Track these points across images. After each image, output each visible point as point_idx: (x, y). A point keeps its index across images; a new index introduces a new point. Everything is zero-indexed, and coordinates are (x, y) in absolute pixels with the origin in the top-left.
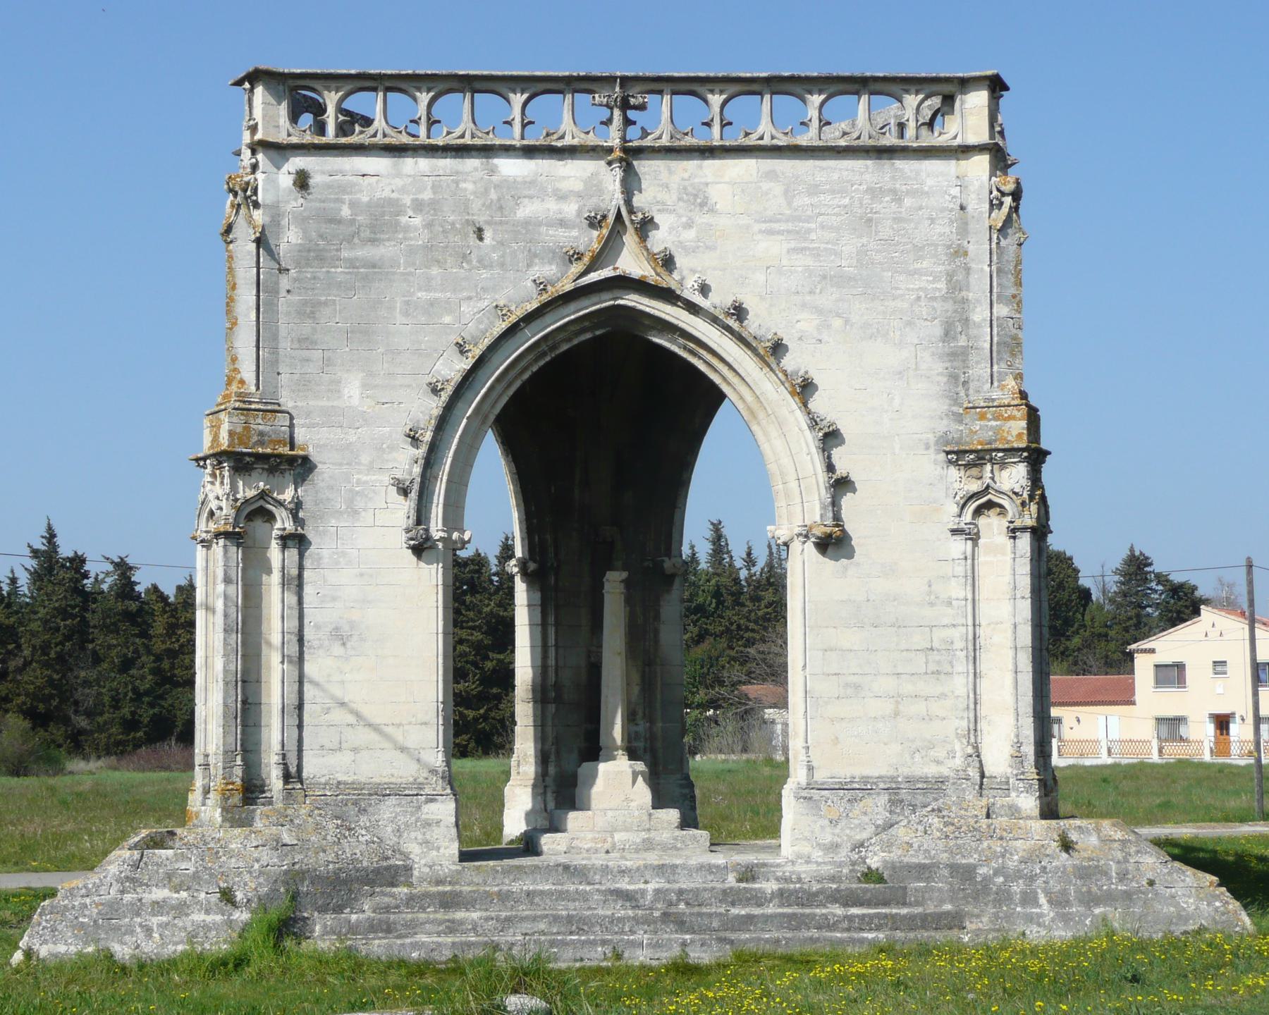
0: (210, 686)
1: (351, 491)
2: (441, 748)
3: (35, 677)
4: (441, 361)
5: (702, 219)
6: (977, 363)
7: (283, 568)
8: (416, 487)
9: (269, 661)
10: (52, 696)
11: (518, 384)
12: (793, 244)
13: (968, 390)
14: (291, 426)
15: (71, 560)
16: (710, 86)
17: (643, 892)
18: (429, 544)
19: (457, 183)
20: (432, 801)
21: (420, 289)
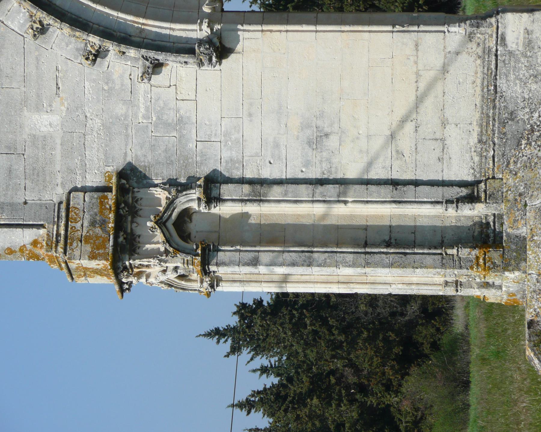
0: (370, 279)
1: (156, 126)
2: (444, 28)
3: (365, 356)
4: (9, 23)
7: (242, 201)
8: (152, 54)
9: (344, 217)
10: (386, 340)
14: (84, 190)
15: (242, 318)
18: (216, 40)
20: (503, 39)
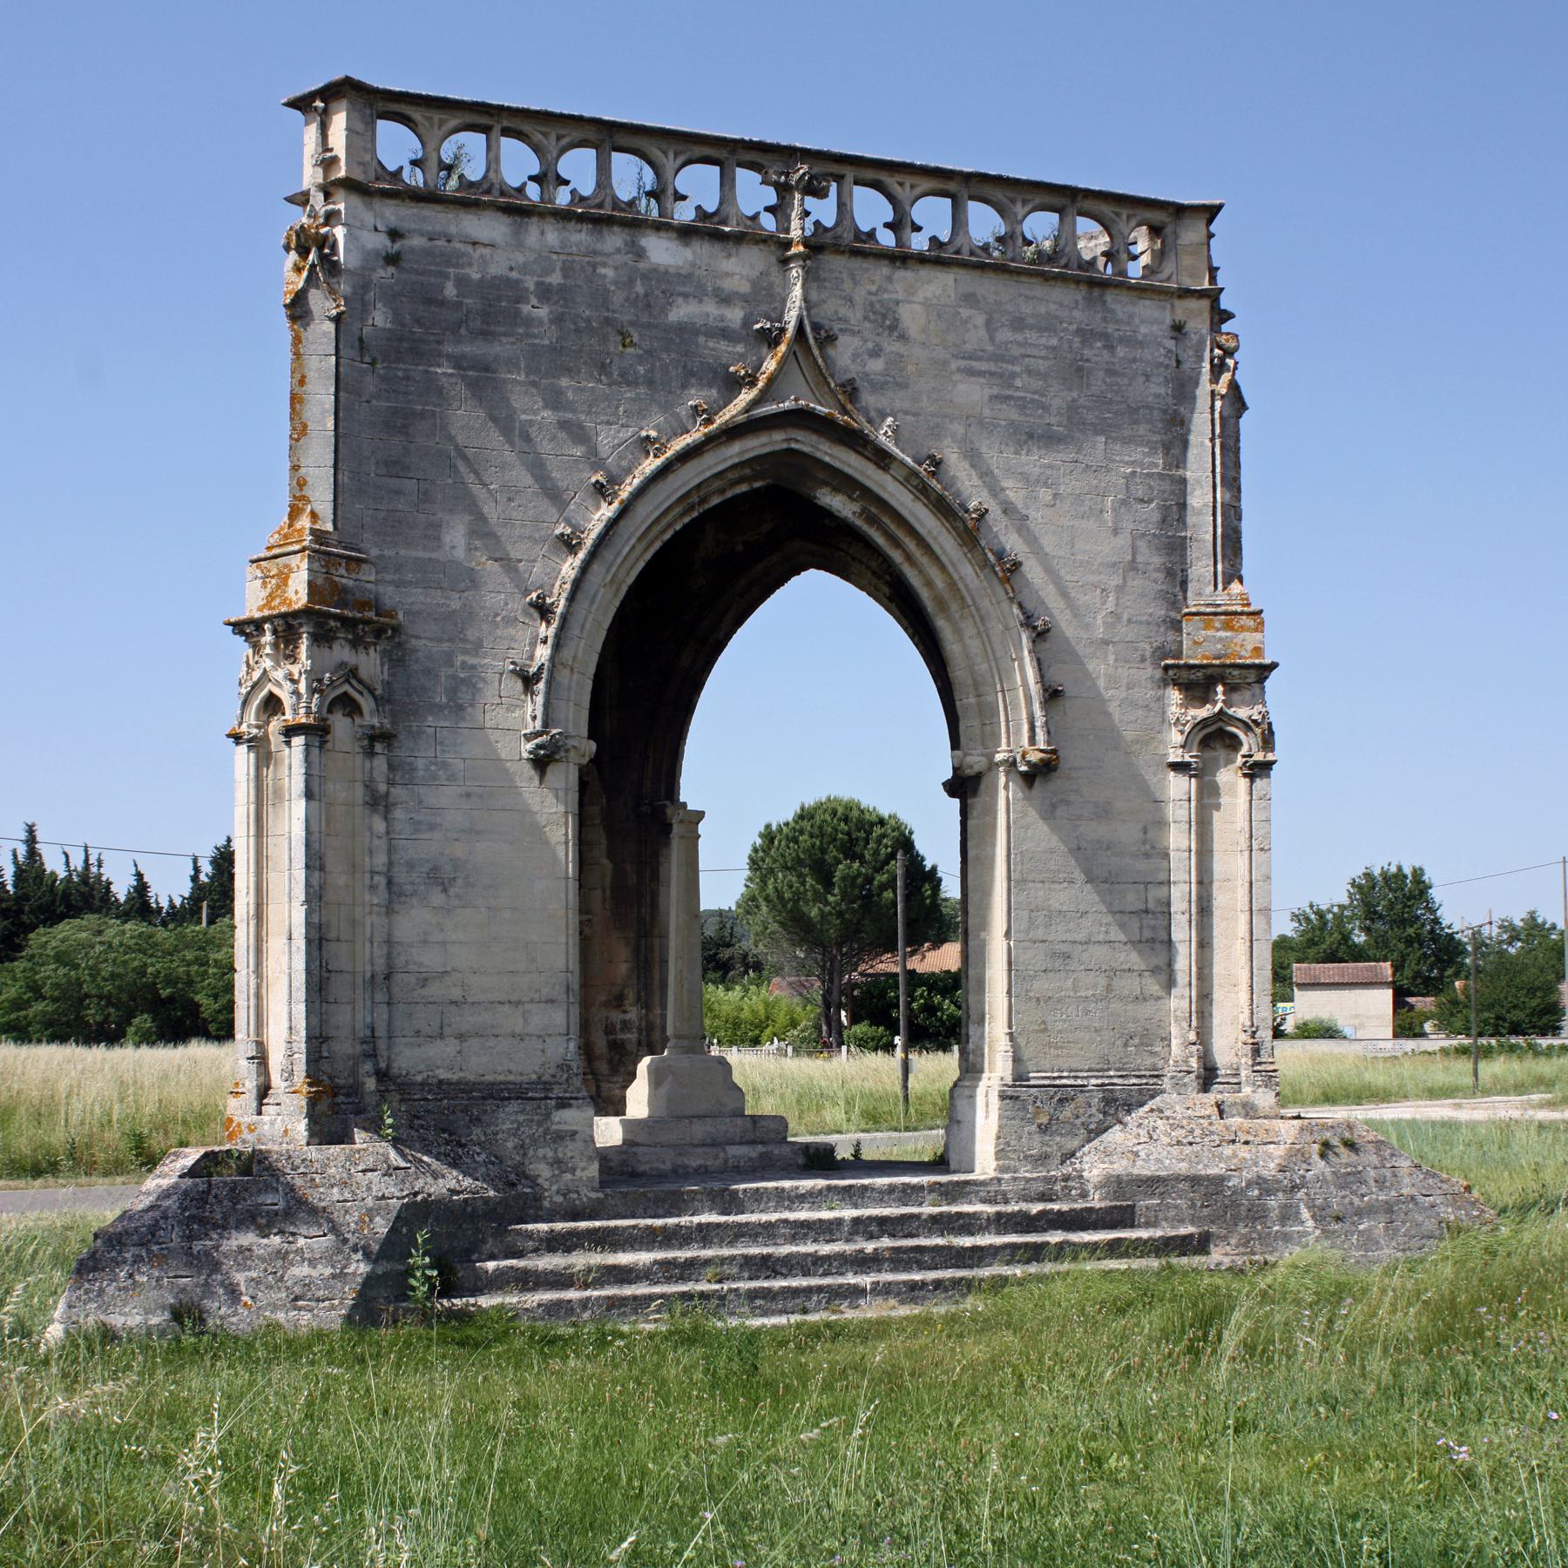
5: (891, 346)
11: (658, 545)
12: (995, 391)
19: (594, 267)
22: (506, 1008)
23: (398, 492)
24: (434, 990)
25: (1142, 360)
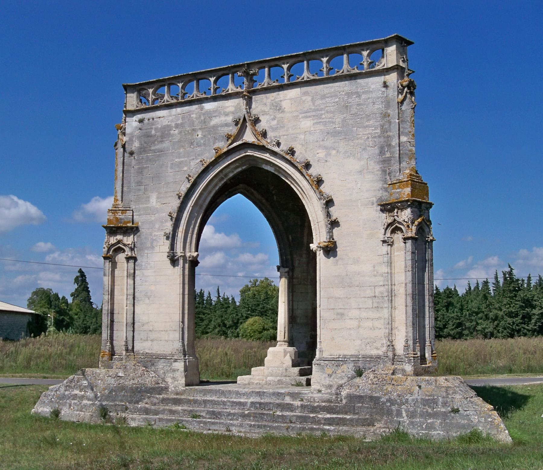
6: (394, 164)
8: (171, 236)
12: (315, 121)
13: (390, 176)
14: (133, 216)
16: (282, 61)
17: (246, 403)
21: (176, 158)
22: (163, 332)
23: (140, 190)
24: (146, 327)
25: (372, 98)
